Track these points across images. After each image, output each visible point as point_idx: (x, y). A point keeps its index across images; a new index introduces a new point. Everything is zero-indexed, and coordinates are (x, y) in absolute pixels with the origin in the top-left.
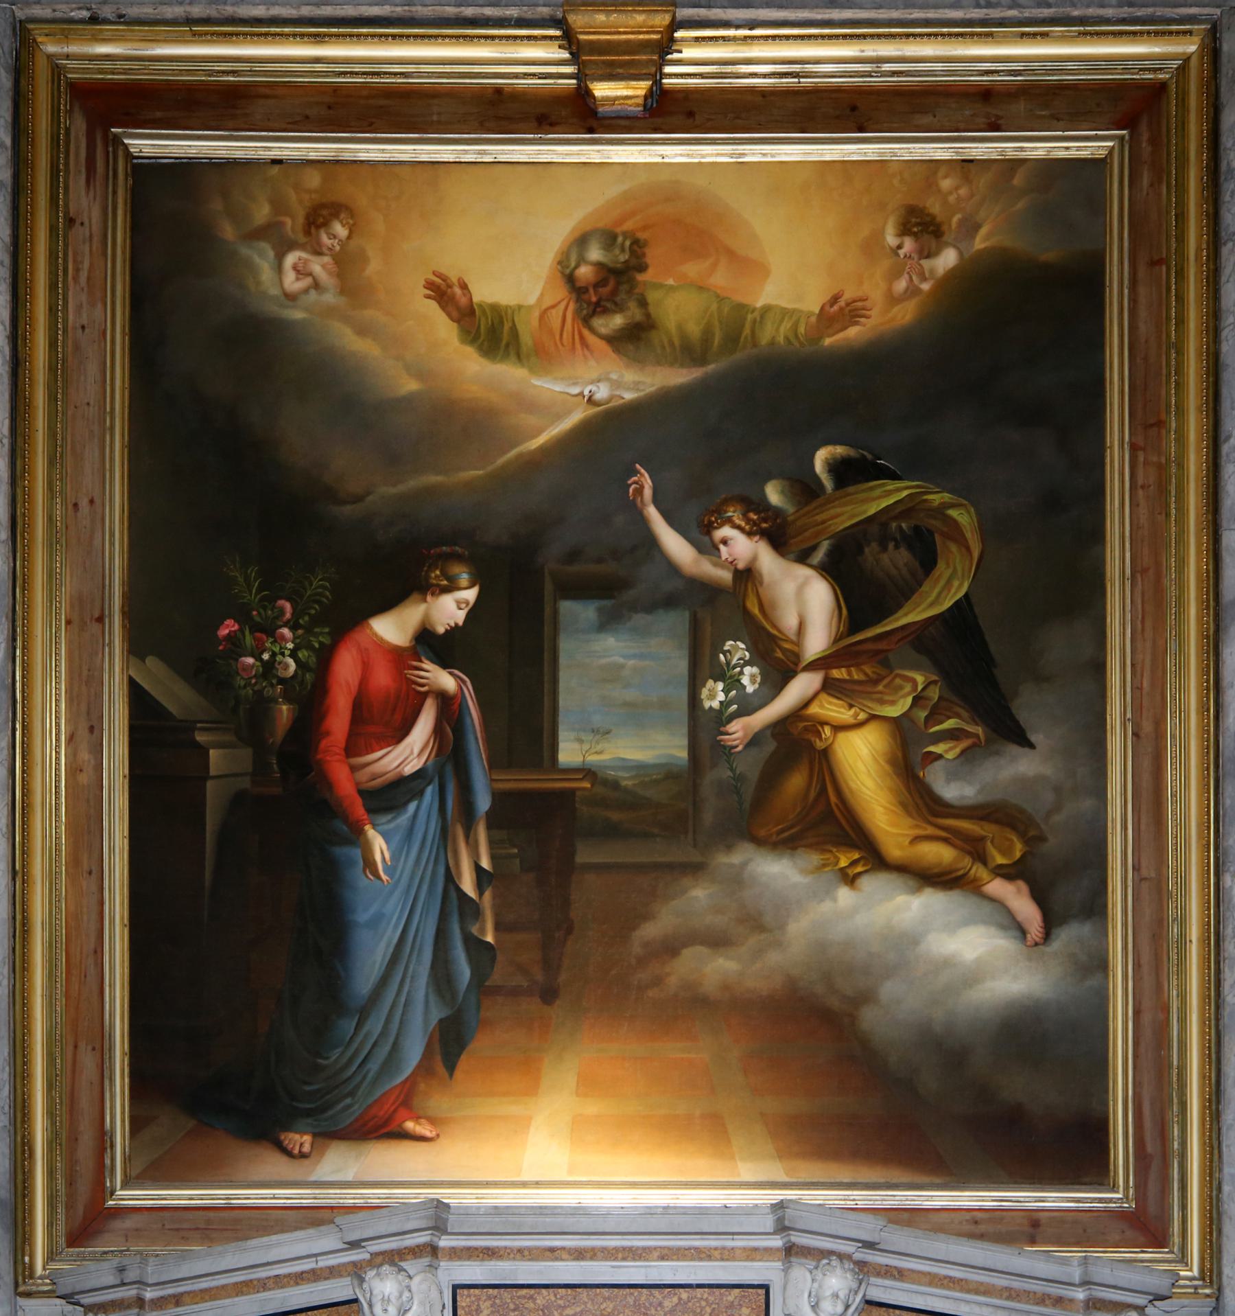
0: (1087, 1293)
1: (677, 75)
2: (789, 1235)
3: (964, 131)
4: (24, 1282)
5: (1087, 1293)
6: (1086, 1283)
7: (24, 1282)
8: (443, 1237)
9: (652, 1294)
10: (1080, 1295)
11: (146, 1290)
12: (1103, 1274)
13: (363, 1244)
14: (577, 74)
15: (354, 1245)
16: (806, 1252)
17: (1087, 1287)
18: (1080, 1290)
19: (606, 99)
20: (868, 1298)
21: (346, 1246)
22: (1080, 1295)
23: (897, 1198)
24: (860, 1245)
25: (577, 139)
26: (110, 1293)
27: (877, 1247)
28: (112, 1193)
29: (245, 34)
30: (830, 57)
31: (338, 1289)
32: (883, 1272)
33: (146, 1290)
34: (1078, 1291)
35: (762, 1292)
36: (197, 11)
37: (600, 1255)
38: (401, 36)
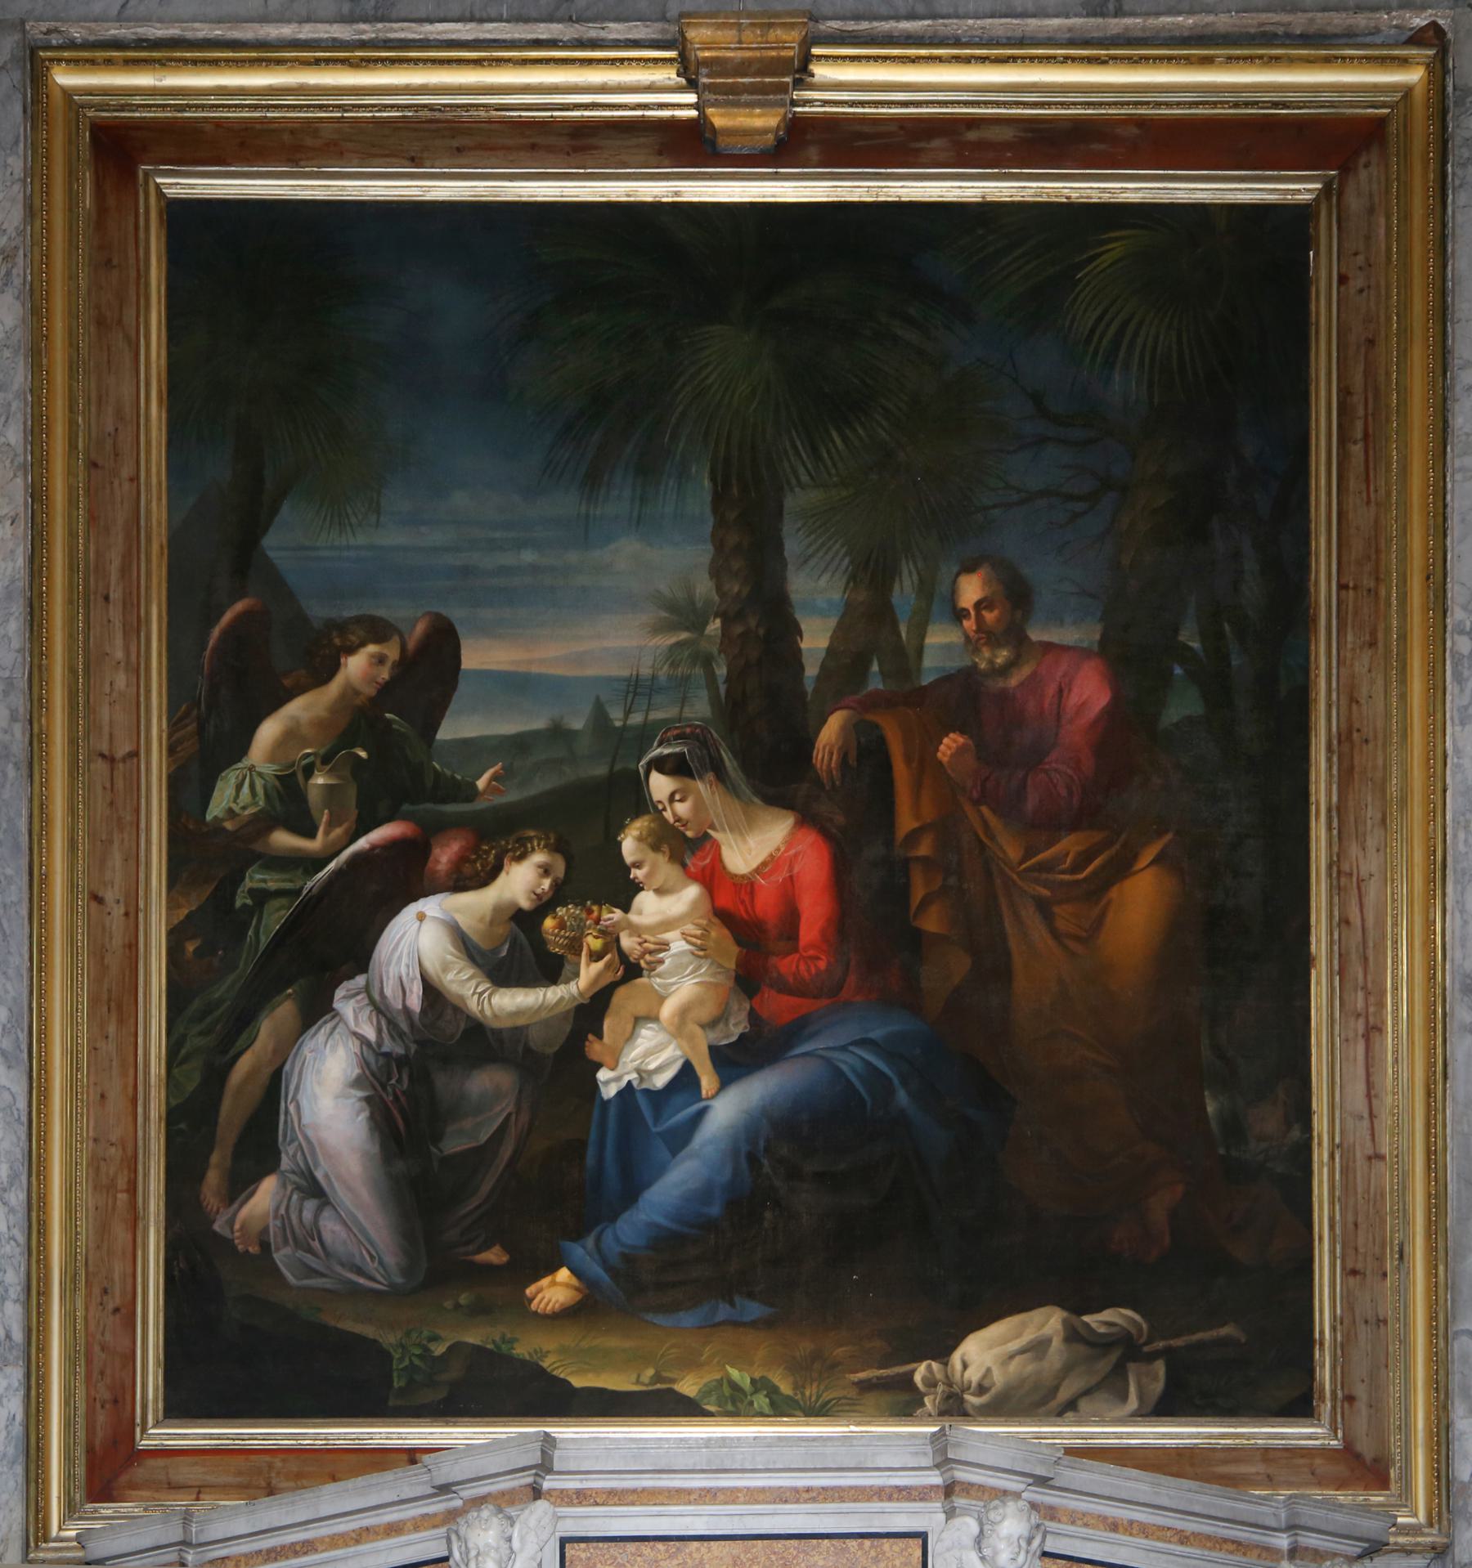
0: (1292, 1539)
1: (814, 102)
2: (952, 1469)
3: (698, 172)
4: (37, 1546)
5: (1292, 1539)
6: (1292, 1528)
7: (37, 1546)
8: (548, 1477)
9: (845, 1550)
10: (1283, 1542)
11: (189, 1553)
12: (1309, 1514)
13: (454, 1488)
14: (697, 103)
15: (444, 1489)
16: (968, 1488)
17: (1293, 1532)
18: (1285, 1536)
19: (730, 132)
20: (1047, 1549)
21: (435, 1491)
22: (1283, 1542)
23: (434, 1436)
24: (1030, 1481)
25: (799, 174)
26: (1219, 1526)
27: (1050, 1483)
28: (144, 1430)
29: (383, 60)
30: (1129, 83)
31: (425, 1546)
32: (364, 1534)
33: (189, 1553)
34: (1283, 1538)
35: (915, 1546)
36: (1223, 22)
37: (721, 1497)
38: (622, 60)
